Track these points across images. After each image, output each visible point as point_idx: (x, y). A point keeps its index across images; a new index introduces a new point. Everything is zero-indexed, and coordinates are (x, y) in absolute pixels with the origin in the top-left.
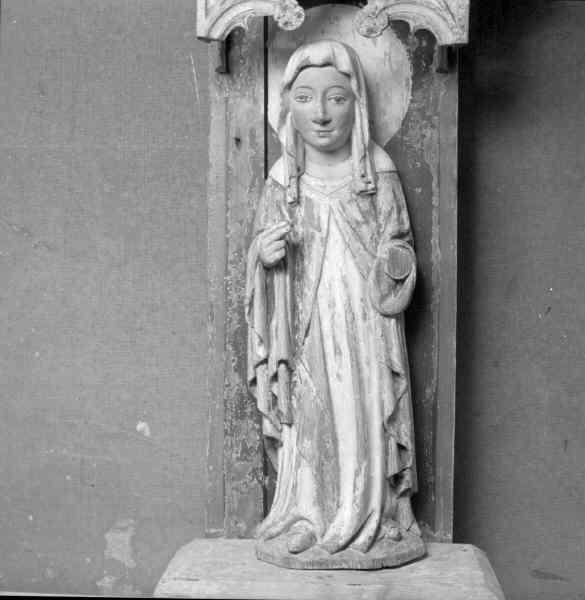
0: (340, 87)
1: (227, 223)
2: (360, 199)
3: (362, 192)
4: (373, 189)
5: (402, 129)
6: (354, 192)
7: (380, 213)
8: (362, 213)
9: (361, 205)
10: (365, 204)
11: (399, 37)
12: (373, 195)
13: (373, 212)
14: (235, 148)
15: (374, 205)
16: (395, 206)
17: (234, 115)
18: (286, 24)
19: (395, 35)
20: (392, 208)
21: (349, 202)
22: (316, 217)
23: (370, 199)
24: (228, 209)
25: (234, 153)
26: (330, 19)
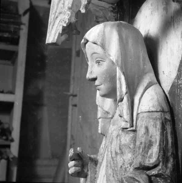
2: (123, 134)
5: (178, 74)
23: (132, 135)
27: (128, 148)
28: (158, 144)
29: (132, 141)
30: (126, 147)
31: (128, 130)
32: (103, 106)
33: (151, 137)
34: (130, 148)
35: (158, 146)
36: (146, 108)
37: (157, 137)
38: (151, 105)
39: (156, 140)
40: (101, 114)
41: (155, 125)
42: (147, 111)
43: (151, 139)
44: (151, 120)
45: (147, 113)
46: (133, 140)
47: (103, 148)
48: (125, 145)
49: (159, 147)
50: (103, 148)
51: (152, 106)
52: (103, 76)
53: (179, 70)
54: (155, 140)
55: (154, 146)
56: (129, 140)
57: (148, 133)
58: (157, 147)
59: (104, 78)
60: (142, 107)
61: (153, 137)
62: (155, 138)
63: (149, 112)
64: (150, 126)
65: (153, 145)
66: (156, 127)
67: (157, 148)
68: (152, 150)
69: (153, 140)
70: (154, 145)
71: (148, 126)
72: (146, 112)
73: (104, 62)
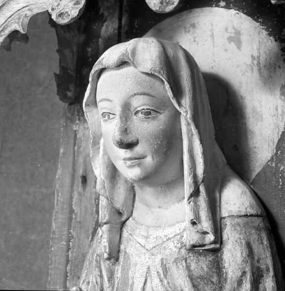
0: (144, 94)
1: (66, 280)
2: (192, 258)
3: (194, 246)
4: (214, 242)
5: (276, 154)
6: (183, 245)
7: (226, 279)
8: (191, 278)
9: (193, 266)
10: (200, 266)
11: (270, 35)
12: (216, 250)
13: (215, 279)
14: (80, 189)
15: (218, 267)
16: (248, 269)
17: (82, 149)
18: (61, 15)
19: (265, 33)
20: (244, 273)
21: (176, 261)
22: (130, 282)
23: (210, 258)
24: (68, 261)
25: (80, 194)
26: (185, 28)
27: (210, 283)
28: (271, 273)
29: (214, 270)
30: (205, 281)
31: (206, 248)
32: (113, 199)
33: (258, 261)
34: (212, 282)
35: (272, 277)
36: (239, 209)
37: (268, 261)
38: (247, 204)
39: (266, 267)
40: (109, 215)
41: (261, 239)
42: (243, 214)
43: (258, 265)
44: (253, 231)
45: (242, 218)
46: (215, 267)
47: (99, 283)
48: (201, 278)
49: (275, 279)
50: (99, 283)
51: (249, 205)
52: (156, 143)
53: (278, 147)
54: (265, 266)
55: (265, 277)
56: (207, 267)
57: (252, 254)
58: (271, 278)
59: (156, 146)
60: (227, 206)
61: (261, 262)
62: (264, 263)
63: (246, 216)
64: (254, 241)
65: (263, 276)
66: (262, 243)
67: (273, 281)
68: (264, 284)
69: (263, 267)
70: (265, 275)
71: (249, 241)
72: (240, 216)
73: (158, 114)
